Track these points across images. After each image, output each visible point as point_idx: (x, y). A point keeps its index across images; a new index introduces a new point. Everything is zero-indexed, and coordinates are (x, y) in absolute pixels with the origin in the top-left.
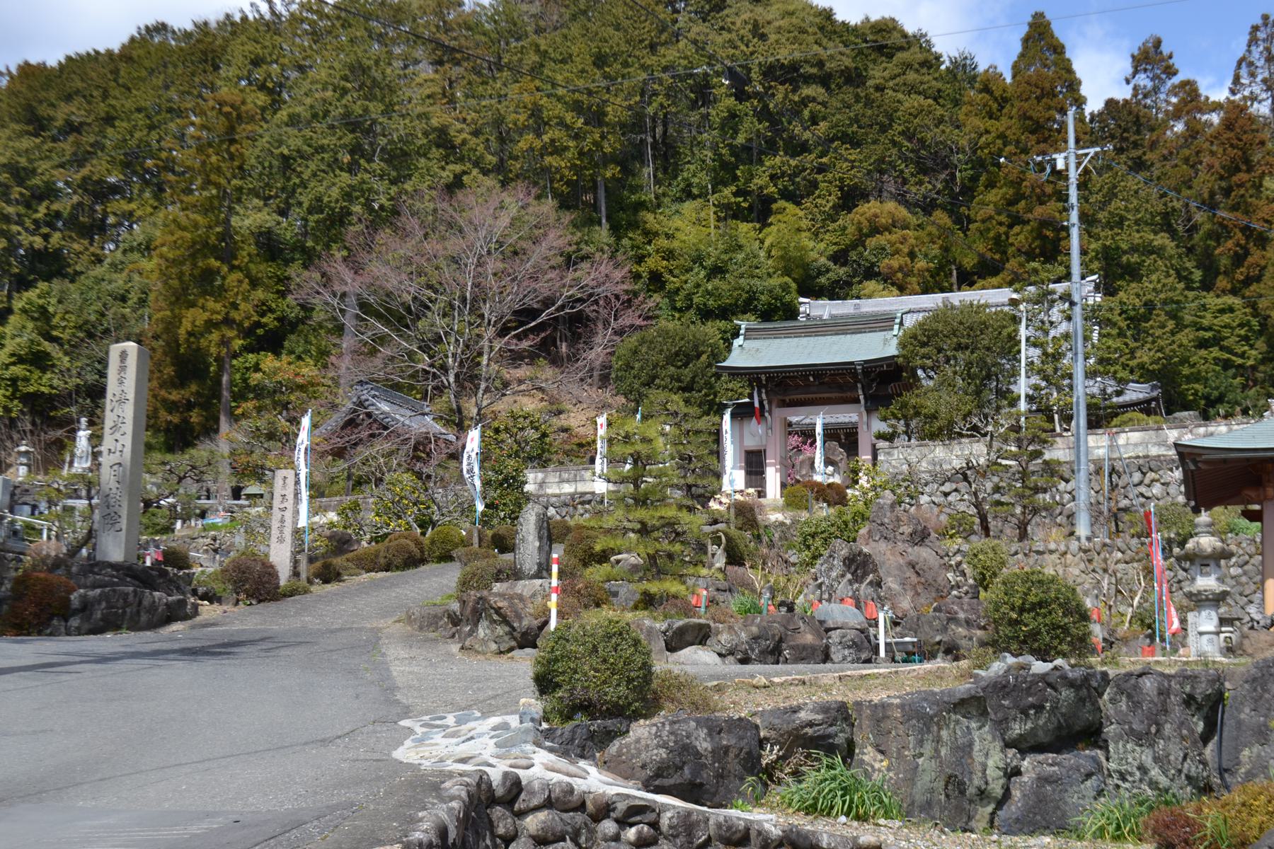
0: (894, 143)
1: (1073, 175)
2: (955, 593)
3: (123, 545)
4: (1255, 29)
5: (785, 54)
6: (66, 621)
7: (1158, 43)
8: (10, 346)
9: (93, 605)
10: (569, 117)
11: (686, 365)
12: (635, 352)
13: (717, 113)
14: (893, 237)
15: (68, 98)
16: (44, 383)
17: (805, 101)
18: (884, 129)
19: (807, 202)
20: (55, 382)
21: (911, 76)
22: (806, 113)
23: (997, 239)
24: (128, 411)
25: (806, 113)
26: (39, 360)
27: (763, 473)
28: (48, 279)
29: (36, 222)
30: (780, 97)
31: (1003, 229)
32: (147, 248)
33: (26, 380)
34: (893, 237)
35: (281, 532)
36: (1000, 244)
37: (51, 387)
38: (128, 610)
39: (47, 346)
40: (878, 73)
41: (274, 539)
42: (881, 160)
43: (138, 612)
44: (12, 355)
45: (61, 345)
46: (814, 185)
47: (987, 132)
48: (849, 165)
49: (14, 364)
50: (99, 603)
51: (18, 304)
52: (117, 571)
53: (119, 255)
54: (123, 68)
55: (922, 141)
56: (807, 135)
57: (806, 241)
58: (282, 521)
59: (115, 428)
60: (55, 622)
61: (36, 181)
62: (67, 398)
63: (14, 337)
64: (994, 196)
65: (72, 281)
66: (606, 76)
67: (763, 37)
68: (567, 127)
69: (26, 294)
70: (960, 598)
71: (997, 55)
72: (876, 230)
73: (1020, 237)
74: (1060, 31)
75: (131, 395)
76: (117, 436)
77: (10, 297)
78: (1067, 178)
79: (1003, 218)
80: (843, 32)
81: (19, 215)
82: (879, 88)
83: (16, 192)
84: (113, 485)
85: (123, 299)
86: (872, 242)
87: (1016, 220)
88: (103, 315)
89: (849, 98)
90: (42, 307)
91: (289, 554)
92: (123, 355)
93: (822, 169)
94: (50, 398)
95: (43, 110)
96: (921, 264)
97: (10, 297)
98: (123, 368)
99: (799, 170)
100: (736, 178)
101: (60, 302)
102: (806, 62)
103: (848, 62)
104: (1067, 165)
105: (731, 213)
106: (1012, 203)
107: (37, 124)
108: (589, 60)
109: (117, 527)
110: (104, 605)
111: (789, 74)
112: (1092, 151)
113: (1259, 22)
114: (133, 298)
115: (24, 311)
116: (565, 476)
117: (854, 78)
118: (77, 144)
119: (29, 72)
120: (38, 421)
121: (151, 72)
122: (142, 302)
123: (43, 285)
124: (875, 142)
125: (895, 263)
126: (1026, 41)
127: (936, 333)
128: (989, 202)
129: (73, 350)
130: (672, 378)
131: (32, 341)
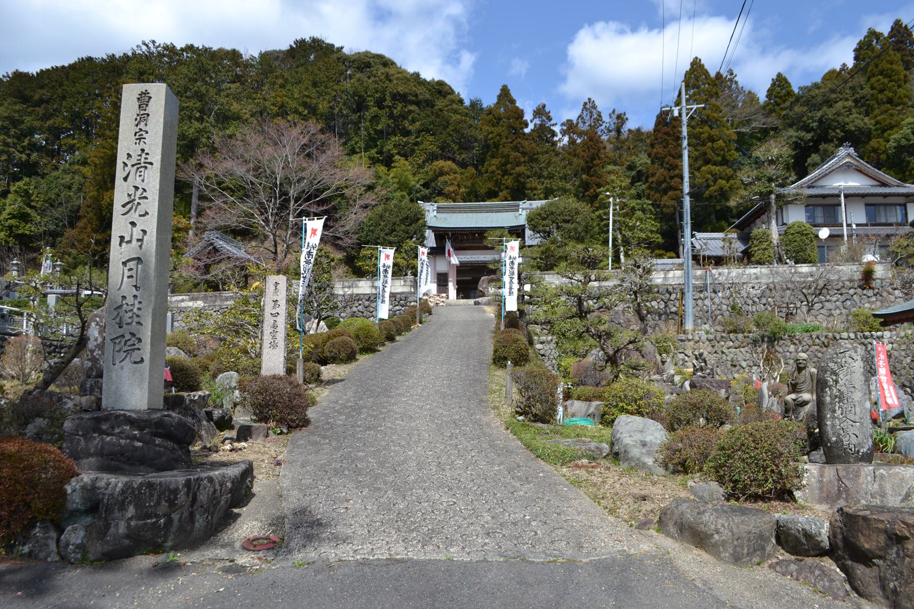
0: (450, 135)
1: (685, 119)
2: (699, 374)
3: (146, 385)
4: (585, 104)
5: (401, 89)
6: (61, 531)
7: (544, 106)
8: (8, 210)
9: (109, 510)
10: (301, 109)
11: (410, 224)
12: (381, 216)
13: (368, 115)
14: (451, 177)
15: (42, 87)
16: (27, 229)
17: (411, 112)
18: (445, 127)
19: (410, 159)
20: (33, 229)
21: (455, 106)
22: (410, 118)
23: (496, 181)
24: (152, 180)
25: (410, 118)
26: (24, 217)
27: (447, 285)
28: (30, 176)
29: (23, 147)
30: (399, 108)
31: (499, 177)
32: (84, 163)
33: (17, 227)
34: (451, 177)
35: (274, 338)
36: (498, 183)
37: (31, 231)
38: (175, 516)
39: (28, 210)
40: (440, 103)
41: (266, 344)
42: (444, 142)
43: (192, 515)
44: (9, 214)
45: (36, 211)
46: (413, 151)
47: (492, 133)
48: (430, 144)
49: (10, 219)
50: (123, 507)
51: (12, 189)
52: (141, 429)
53: (67, 166)
54: (71, 73)
55: (463, 134)
56: (411, 128)
57: (410, 177)
58: (275, 326)
59: (130, 204)
60: (37, 531)
61: (23, 126)
62: (39, 237)
63: (10, 205)
64: (496, 161)
65: (43, 178)
66: (318, 92)
67: (390, 81)
68: (300, 114)
69: (17, 183)
70: (704, 377)
71: (489, 100)
72: (442, 173)
73: (509, 181)
74: (514, 94)
75: (156, 157)
76: (134, 216)
77: (8, 184)
78: (681, 121)
79: (499, 172)
80: (424, 83)
81: (14, 143)
82: (441, 110)
83: (12, 132)
84: (127, 289)
85: (70, 188)
86: (441, 179)
87: (505, 173)
88: (59, 195)
89: (429, 113)
90: (26, 190)
91: (282, 359)
92: (144, 99)
93: (416, 144)
94: (30, 237)
95: (28, 93)
96: (462, 190)
97: (8, 184)
98: (143, 117)
99: (407, 143)
100: (377, 146)
101: (35, 188)
102: (411, 94)
103: (428, 96)
104: (680, 114)
105: (374, 161)
106: (505, 165)
107: (25, 99)
108: (310, 83)
109: (136, 356)
110: (131, 511)
111: (402, 98)
112: (695, 107)
113: (587, 101)
114: (75, 187)
115: (16, 192)
116: (346, 284)
117: (430, 104)
118: (46, 109)
119: (19, 76)
120: (24, 248)
121: (86, 75)
122: (79, 190)
123: (26, 179)
124: (441, 133)
125: (451, 189)
126: (499, 97)
127: (552, 213)
128: (493, 164)
129: (42, 212)
130: (403, 231)
131: (20, 207)
